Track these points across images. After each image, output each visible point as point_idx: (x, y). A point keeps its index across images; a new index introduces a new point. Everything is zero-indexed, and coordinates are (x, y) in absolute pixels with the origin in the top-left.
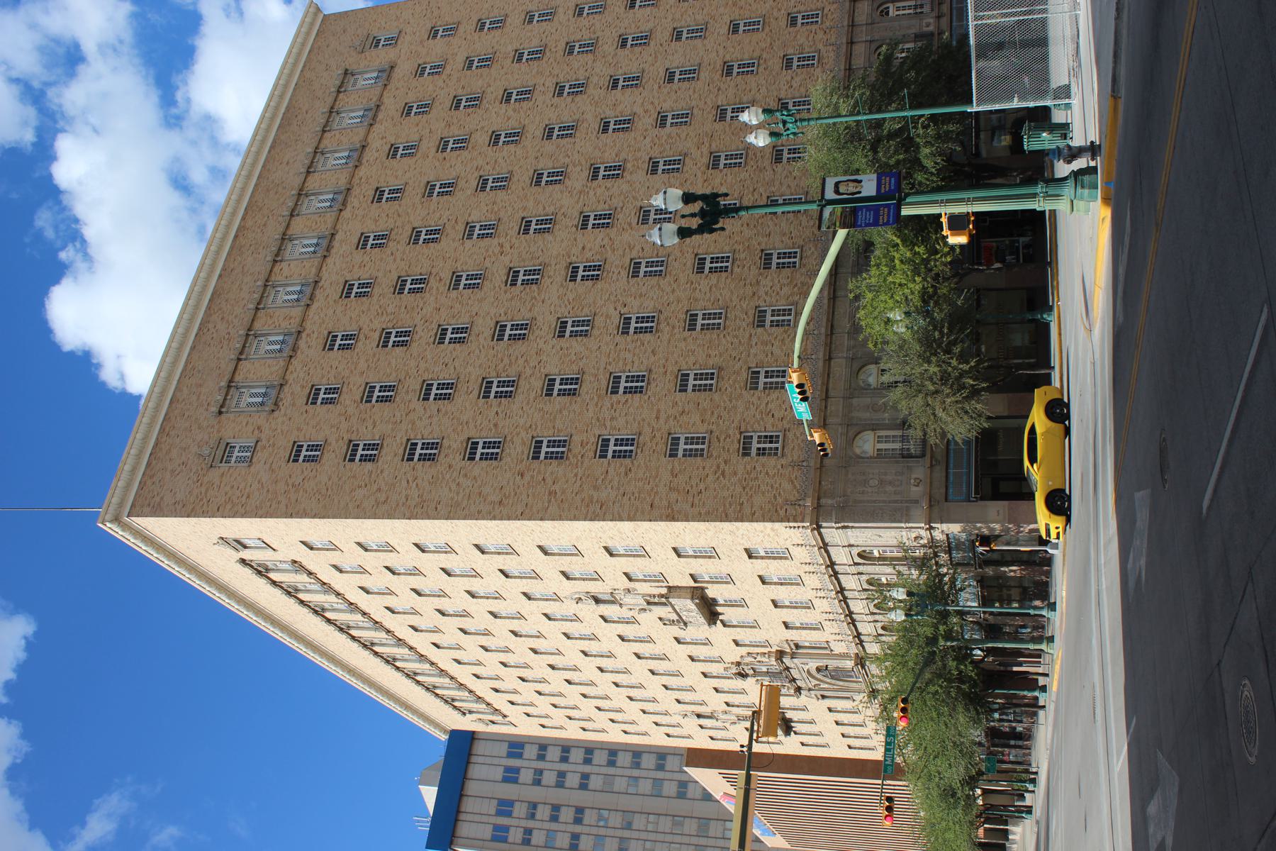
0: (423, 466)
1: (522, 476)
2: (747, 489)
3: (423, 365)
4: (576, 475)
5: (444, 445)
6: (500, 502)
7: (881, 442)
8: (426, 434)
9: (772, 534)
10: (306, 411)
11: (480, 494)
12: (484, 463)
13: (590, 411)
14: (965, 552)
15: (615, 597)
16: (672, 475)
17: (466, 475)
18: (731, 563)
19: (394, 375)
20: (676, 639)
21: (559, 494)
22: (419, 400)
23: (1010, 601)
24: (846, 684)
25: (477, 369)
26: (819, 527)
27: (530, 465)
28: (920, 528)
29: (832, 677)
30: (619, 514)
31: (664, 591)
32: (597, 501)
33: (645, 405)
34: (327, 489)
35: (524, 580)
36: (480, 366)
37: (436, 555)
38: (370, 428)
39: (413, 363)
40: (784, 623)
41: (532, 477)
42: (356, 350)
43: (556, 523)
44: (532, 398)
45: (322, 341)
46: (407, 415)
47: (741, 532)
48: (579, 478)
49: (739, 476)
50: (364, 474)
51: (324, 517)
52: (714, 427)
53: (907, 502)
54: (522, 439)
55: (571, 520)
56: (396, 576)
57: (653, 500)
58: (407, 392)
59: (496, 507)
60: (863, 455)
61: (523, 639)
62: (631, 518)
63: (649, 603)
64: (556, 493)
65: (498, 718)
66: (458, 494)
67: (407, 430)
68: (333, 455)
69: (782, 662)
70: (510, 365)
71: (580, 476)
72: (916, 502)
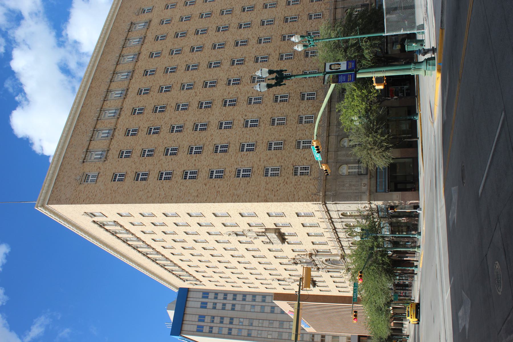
0: (166, 182)
2: (297, 189)
3: (165, 141)
4: (227, 184)
7: (350, 169)
8: (167, 168)
11: (189, 192)
12: (190, 180)
13: (233, 158)
14: (384, 213)
15: (244, 233)
16: (266, 183)
17: (183, 185)
18: (290, 219)
19: (153, 145)
21: (221, 192)
22: (163, 155)
23: (402, 232)
26: (325, 204)
27: (209, 181)
28: (366, 203)
29: (332, 264)
30: (245, 199)
31: (264, 230)
32: (236, 195)
35: (207, 227)
36: (188, 141)
38: (144, 167)
39: (161, 141)
40: (312, 242)
41: (210, 185)
42: (138, 136)
45: (124, 132)
46: (159, 161)
48: (229, 186)
49: (293, 183)
52: (283, 164)
53: (360, 193)
55: (226, 202)
57: (259, 194)
59: (196, 198)
60: (342, 174)
61: (207, 250)
62: (250, 201)
63: (258, 235)
64: (219, 192)
65: (198, 283)
66: (180, 193)
69: (312, 258)
70: (200, 141)
71: (229, 184)
72: (364, 193)
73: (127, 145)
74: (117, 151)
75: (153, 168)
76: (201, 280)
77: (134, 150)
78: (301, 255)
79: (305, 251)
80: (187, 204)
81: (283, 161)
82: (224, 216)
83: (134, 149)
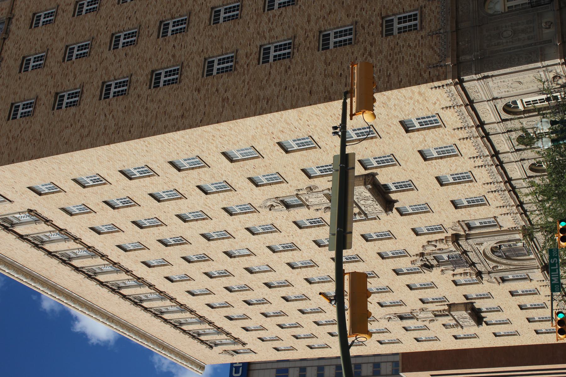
0: (117, 100)
1: (199, 91)
2: (393, 62)
3: (110, 23)
5: (132, 81)
6: (183, 116)
8: (117, 74)
9: (421, 99)
10: (20, 78)
11: (165, 112)
12: (167, 88)
13: (251, 28)
16: (325, 62)
17: (153, 100)
18: (391, 141)
19: (88, 35)
20: (416, 339)
21: (230, 99)
22: (110, 49)
24: (521, 263)
25: (155, 15)
26: (461, 82)
27: (204, 81)
29: (508, 258)
30: (283, 104)
32: (264, 98)
33: (297, 14)
34: (41, 135)
36: (157, 13)
37: (142, 180)
38: (72, 80)
39: (102, 23)
40: (453, 202)
41: (207, 90)
42: (56, 23)
43: (231, 124)
44: (201, 28)
45: (28, 22)
46: (100, 64)
47: (392, 102)
48: (246, 83)
49: (385, 53)
50: (69, 117)
51: (39, 157)
52: (359, 19)
54: (197, 62)
55: (243, 118)
56: (116, 210)
57: (311, 88)
58: (100, 45)
59: (179, 120)
61: (237, 259)
63: (436, 316)
64: (228, 99)
65: (238, 347)
66: (147, 116)
67: (102, 75)
68: (44, 107)
69: (460, 245)
70: (182, 6)
71: (247, 81)
72: (550, 41)
73: (35, 44)
74: (16, 60)
75: (90, 78)
76: (244, 340)
77: (49, 52)
78: (433, 243)
79: (439, 229)
80: (162, 135)
81: (358, 12)
82: (248, 159)
83: (50, 49)
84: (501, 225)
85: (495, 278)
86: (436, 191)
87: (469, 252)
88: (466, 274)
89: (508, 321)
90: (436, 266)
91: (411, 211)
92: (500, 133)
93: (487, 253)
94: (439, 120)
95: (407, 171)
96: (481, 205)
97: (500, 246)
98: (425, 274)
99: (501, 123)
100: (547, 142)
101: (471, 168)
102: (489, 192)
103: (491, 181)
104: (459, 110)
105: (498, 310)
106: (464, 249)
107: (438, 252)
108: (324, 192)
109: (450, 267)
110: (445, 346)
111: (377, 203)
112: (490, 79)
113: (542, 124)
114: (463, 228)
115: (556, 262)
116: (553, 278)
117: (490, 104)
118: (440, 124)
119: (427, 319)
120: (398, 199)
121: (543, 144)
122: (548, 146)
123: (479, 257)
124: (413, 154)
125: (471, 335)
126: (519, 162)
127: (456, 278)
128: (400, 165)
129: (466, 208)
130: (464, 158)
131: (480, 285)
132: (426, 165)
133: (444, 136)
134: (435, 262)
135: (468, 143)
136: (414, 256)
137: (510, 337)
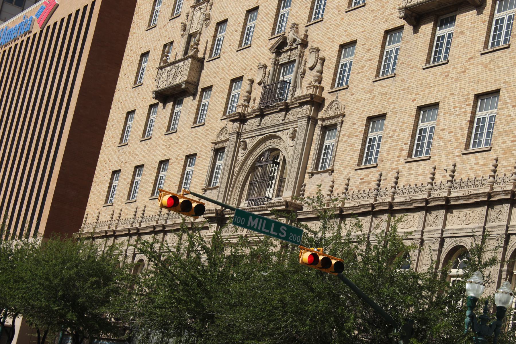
24: (239, 184)
29: (253, 169)
31: (200, 55)
63: (190, 36)
69: (301, 105)
78: (318, 67)
84: (315, 176)
85: (227, 140)
86: (412, 97)
87: (286, 114)
88: (248, 100)
89: (123, 143)
90: (276, 60)
91: (388, 48)
92: (485, 224)
93: (272, 141)
94: (477, 149)
95: (467, 61)
96: (361, 157)
97: (278, 164)
98: (267, 39)
99: (504, 232)
100: (477, 291)
101: (435, 161)
102: (381, 175)
103: (145, 215)
104: (387, 193)
105: (170, 129)
106: (293, 110)
107: (301, 70)
108: (198, 35)
109: (268, 80)
110: (135, 35)
111: (167, 86)
112: (438, 248)
113: (506, 293)
114: (329, 118)
115: (280, 234)
116: (257, 219)
117: (436, 232)
118: (363, 164)
119: (189, 22)
120: (419, 34)
121: (476, 283)
122: (469, 290)
123: (270, 127)
124: (495, 81)
125: (141, 78)
126: (420, 236)
127: (245, 85)
128: (482, 54)
129: (365, 133)
130: (457, 156)
131: (220, 115)
132: (467, 95)
133: (513, 137)
134: (283, 59)
135: (486, 172)
136: (307, 31)
137: (121, 132)
